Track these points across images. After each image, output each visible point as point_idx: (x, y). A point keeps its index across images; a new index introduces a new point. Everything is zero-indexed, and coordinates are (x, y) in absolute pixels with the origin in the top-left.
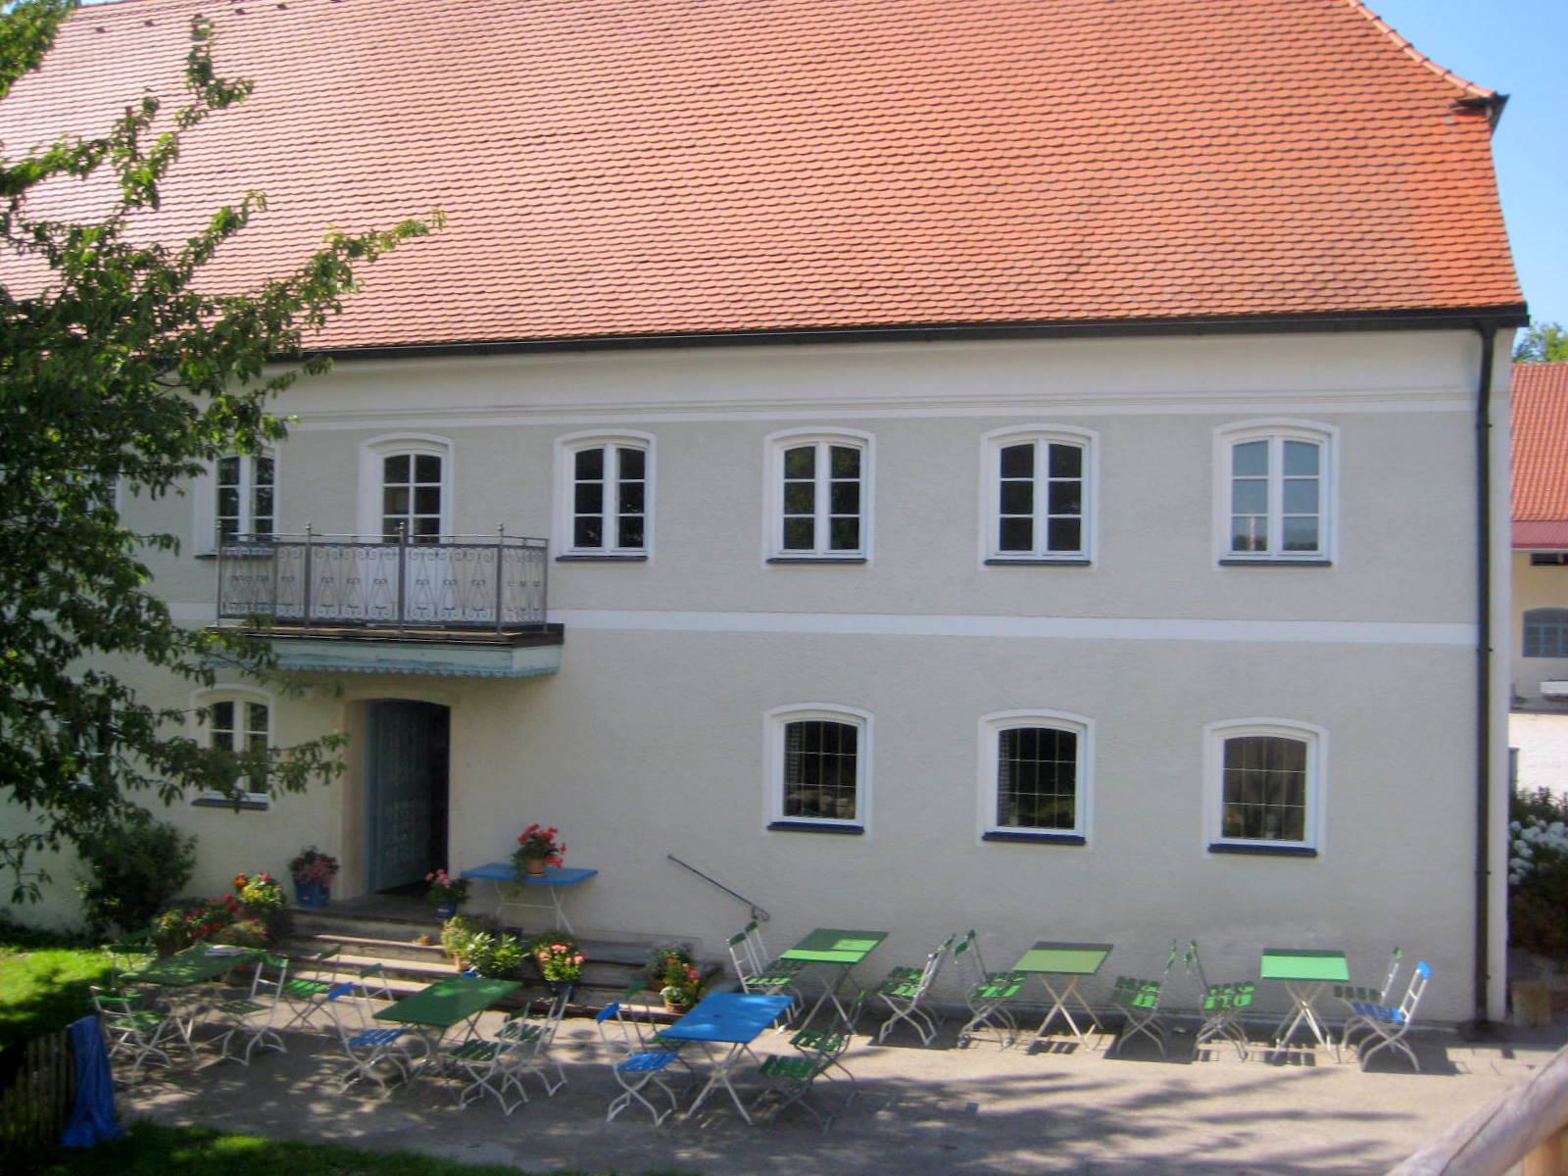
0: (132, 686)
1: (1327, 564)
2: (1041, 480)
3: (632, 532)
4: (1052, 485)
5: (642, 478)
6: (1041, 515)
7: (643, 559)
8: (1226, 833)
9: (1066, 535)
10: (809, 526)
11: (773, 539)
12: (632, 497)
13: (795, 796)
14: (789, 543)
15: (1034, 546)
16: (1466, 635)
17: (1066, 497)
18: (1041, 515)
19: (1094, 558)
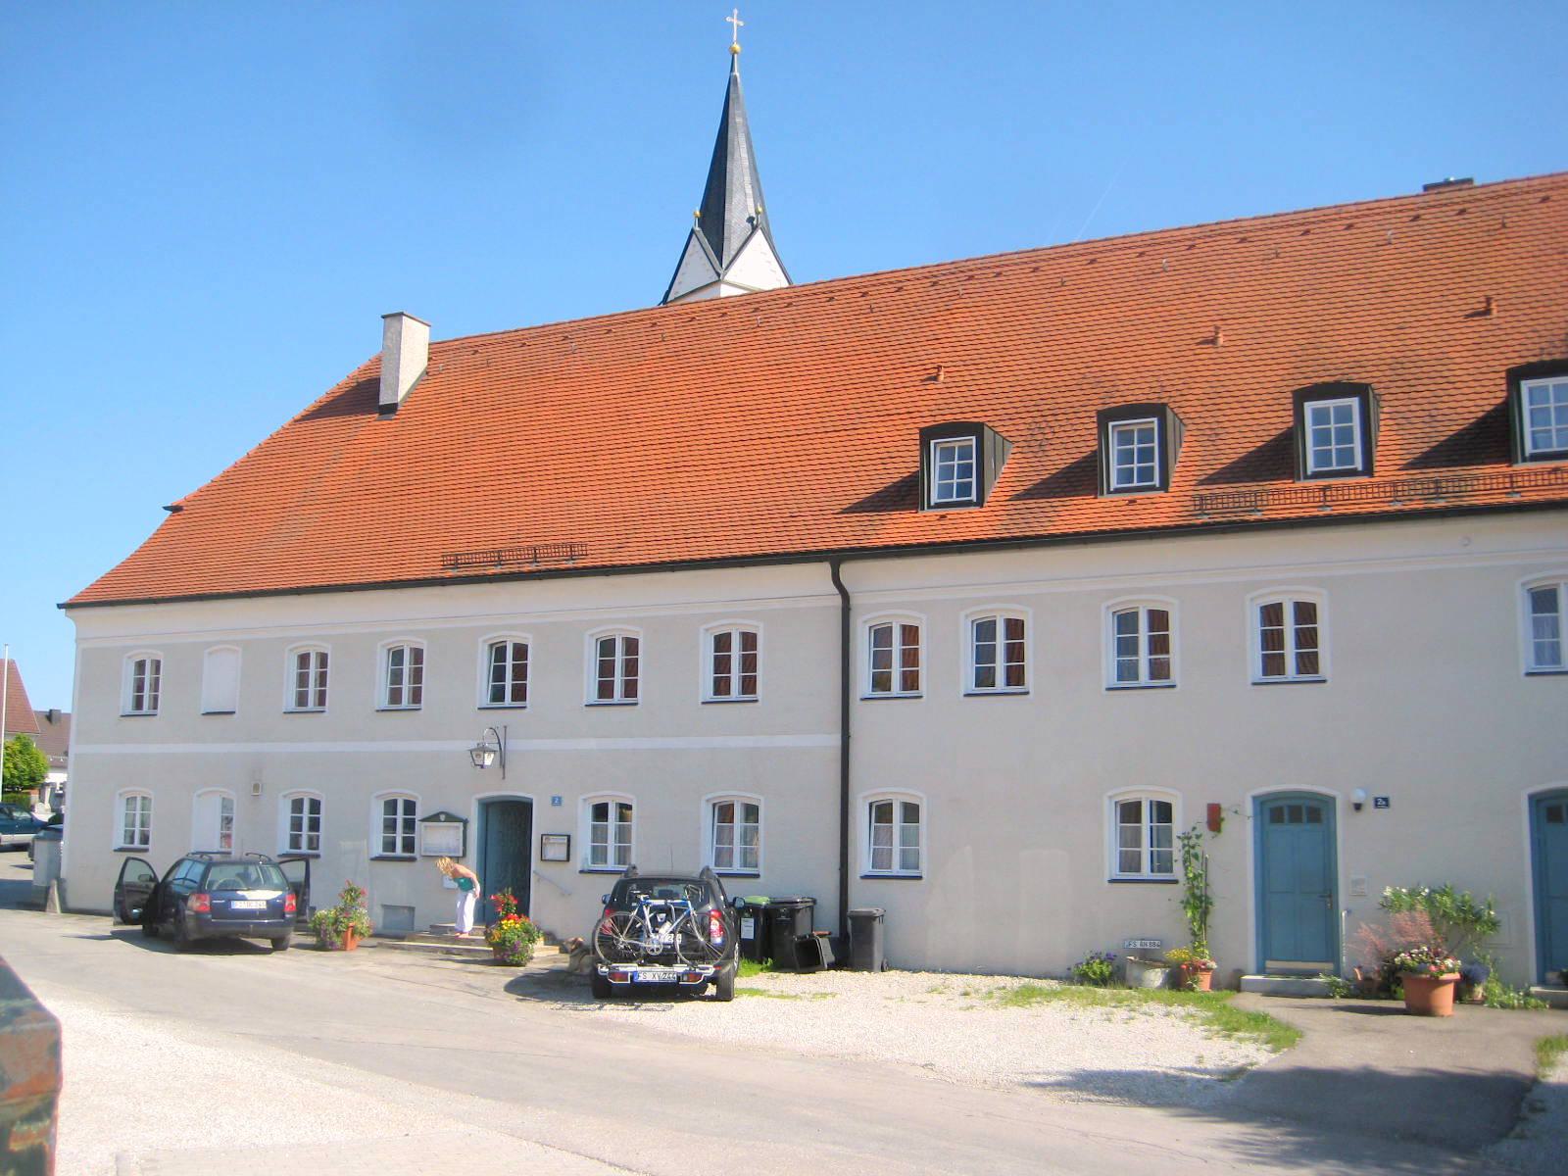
0: (753, 798)
1: (1324, 681)
2: (736, 653)
3: (631, 689)
4: (1297, 631)
5: (1150, 636)
6: (1000, 665)
7: (636, 704)
8: (1122, 870)
9: (1015, 676)
10: (992, 671)
11: (968, 681)
12: (749, 663)
13: (118, 898)
14: (717, 692)
15: (731, 692)
16: (836, 740)
17: (1015, 652)
18: (1290, 651)
19: (1178, 683)
